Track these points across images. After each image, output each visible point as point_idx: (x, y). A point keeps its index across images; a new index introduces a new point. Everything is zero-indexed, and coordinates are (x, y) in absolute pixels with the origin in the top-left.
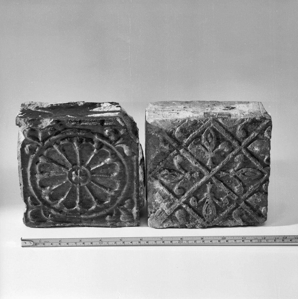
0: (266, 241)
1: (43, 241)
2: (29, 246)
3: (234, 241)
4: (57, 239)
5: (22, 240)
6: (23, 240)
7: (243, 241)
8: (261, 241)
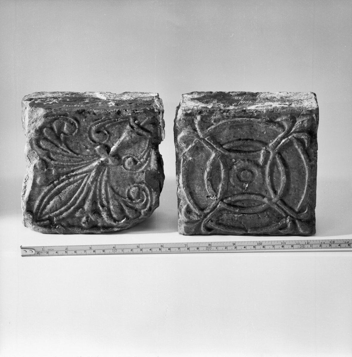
1: (46, 249)
2: (30, 255)
3: (272, 247)
5: (22, 248)
7: (283, 246)
8: (304, 246)
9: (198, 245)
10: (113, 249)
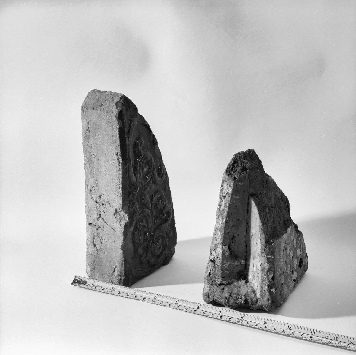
2: (219, 320)
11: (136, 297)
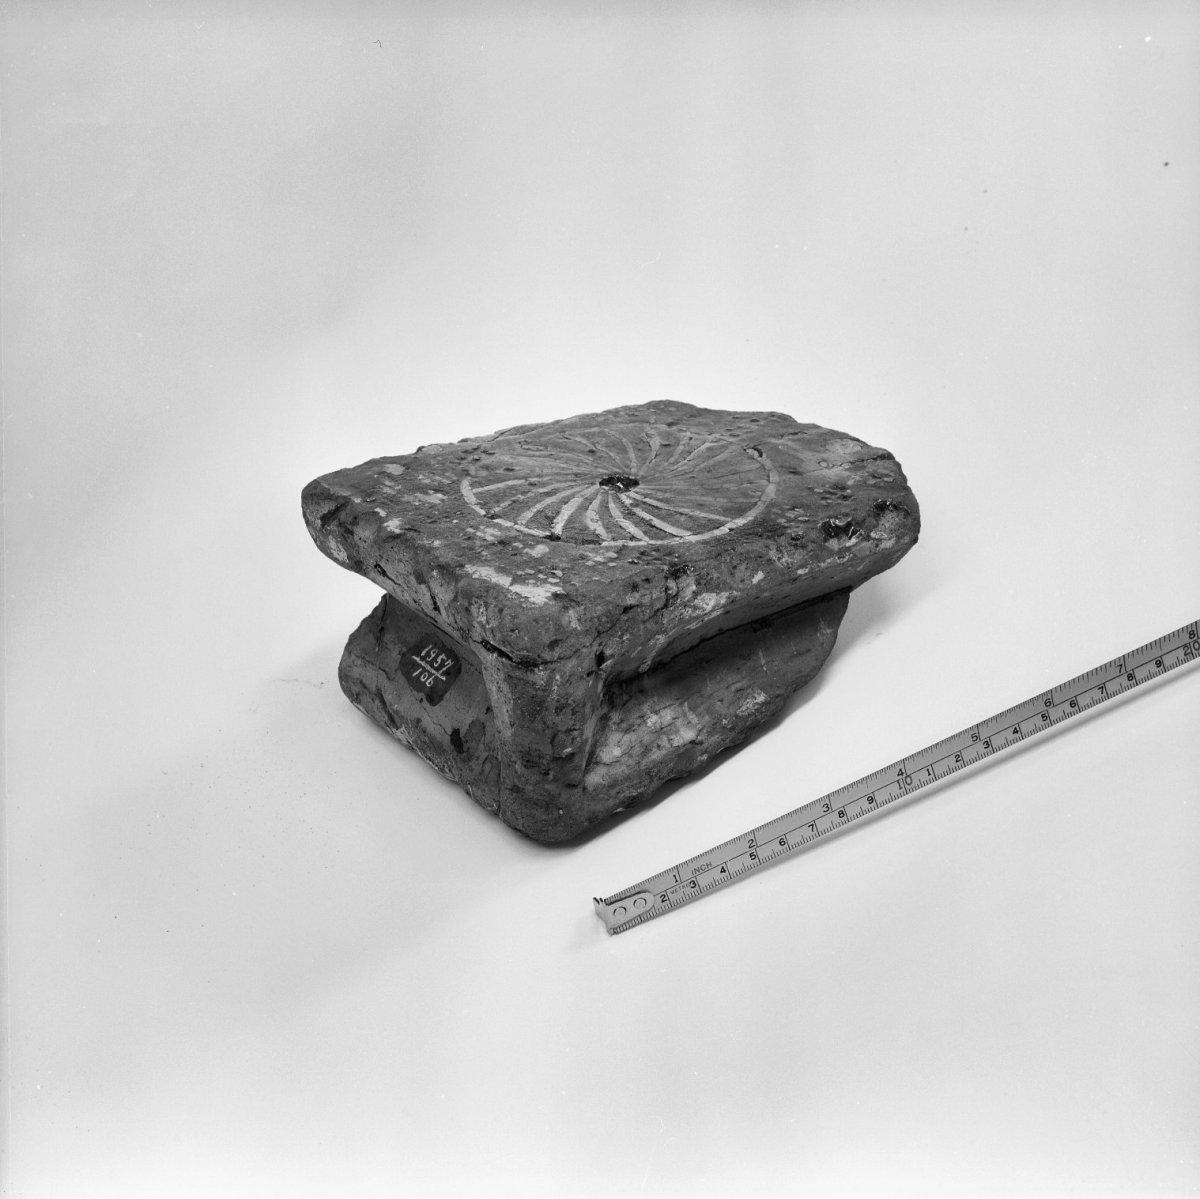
0: (898, 792)
1: (686, 875)
4: (739, 838)
6: (612, 903)
9: (865, 791)
10: (898, 781)
11: (987, 744)
